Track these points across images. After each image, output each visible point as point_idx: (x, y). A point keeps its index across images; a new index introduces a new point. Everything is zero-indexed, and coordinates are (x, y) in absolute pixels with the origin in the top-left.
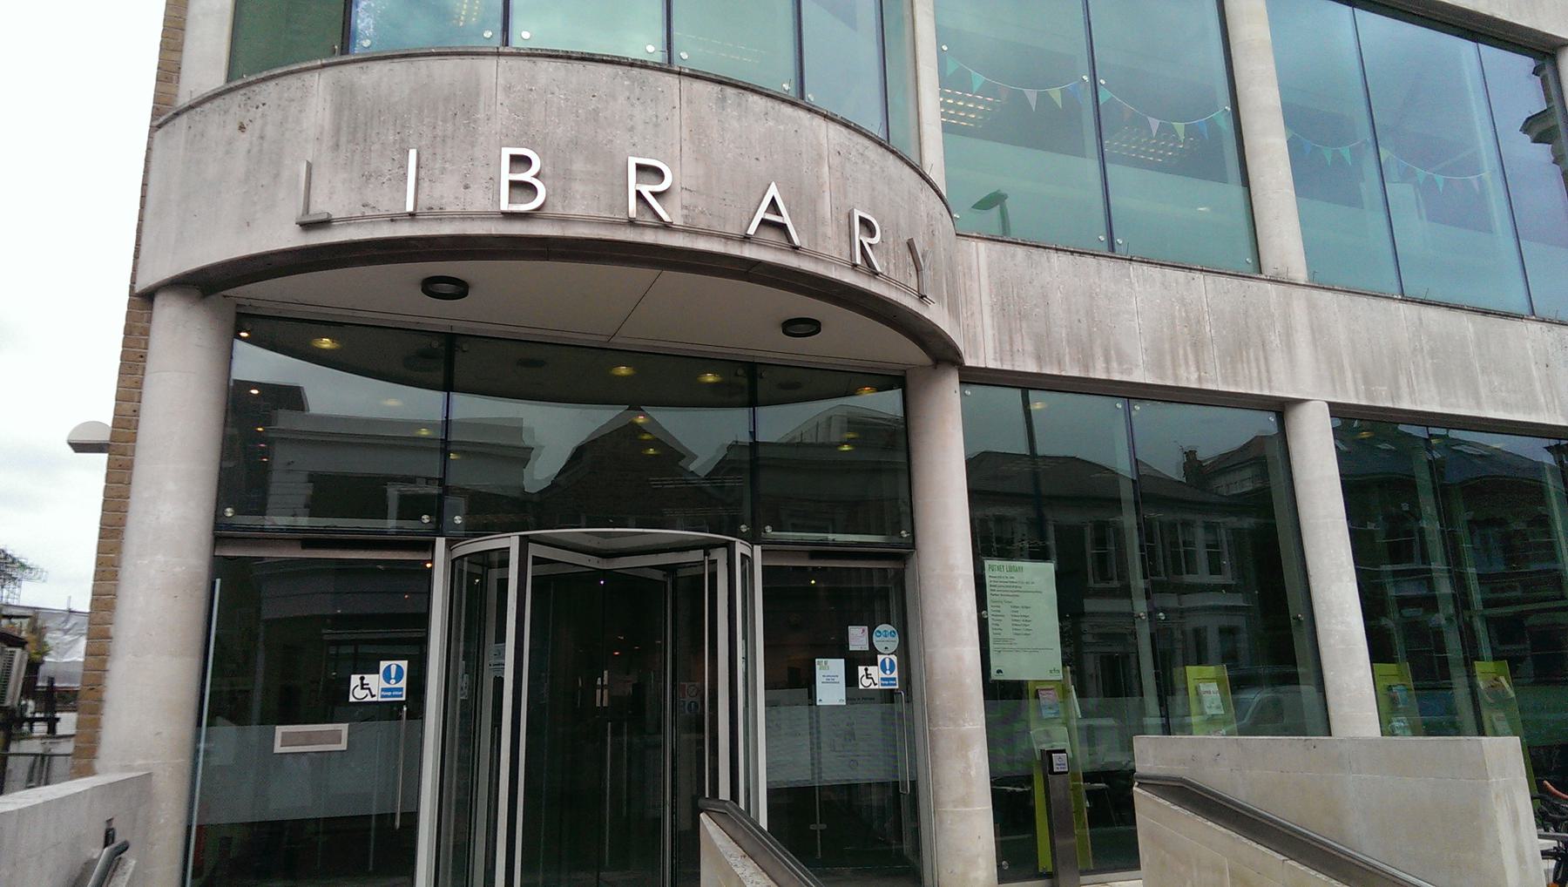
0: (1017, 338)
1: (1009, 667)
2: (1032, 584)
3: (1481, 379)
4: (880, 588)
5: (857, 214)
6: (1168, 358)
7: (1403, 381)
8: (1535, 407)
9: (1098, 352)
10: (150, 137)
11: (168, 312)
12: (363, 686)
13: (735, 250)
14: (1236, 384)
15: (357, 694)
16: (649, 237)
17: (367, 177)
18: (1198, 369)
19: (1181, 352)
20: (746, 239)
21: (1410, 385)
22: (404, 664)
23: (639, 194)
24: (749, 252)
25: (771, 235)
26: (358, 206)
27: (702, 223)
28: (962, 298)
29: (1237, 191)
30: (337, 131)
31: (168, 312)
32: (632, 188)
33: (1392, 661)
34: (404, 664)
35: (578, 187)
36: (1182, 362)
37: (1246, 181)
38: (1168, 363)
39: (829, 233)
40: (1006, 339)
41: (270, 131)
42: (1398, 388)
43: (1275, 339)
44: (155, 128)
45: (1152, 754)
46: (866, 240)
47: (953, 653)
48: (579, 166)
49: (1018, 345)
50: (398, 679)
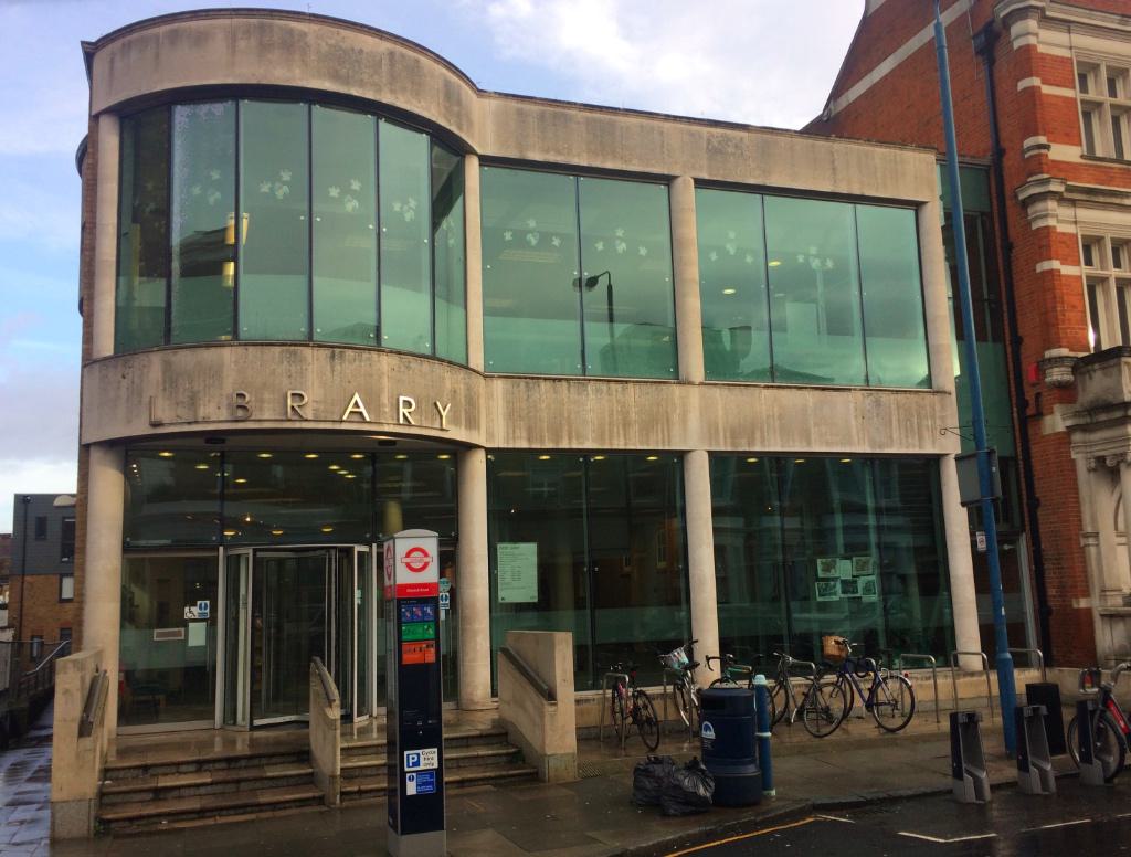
0: (518, 431)
1: (509, 595)
2: (523, 559)
3: (813, 430)
5: (402, 399)
6: (607, 433)
7: (758, 435)
8: (850, 443)
9: (565, 434)
10: (82, 371)
11: (95, 455)
12: (190, 612)
14: (648, 445)
15: (188, 615)
16: (298, 425)
17: (177, 404)
18: (625, 438)
19: (615, 429)
22: (208, 602)
23: (404, 415)
24: (344, 426)
25: (356, 418)
26: (172, 416)
30: (164, 382)
31: (95, 455)
33: (119, 724)
34: (208, 602)
36: (615, 434)
38: (607, 437)
39: (387, 410)
41: (136, 379)
43: (676, 418)
44: (84, 366)
46: (406, 411)
48: (267, 396)
50: (205, 608)
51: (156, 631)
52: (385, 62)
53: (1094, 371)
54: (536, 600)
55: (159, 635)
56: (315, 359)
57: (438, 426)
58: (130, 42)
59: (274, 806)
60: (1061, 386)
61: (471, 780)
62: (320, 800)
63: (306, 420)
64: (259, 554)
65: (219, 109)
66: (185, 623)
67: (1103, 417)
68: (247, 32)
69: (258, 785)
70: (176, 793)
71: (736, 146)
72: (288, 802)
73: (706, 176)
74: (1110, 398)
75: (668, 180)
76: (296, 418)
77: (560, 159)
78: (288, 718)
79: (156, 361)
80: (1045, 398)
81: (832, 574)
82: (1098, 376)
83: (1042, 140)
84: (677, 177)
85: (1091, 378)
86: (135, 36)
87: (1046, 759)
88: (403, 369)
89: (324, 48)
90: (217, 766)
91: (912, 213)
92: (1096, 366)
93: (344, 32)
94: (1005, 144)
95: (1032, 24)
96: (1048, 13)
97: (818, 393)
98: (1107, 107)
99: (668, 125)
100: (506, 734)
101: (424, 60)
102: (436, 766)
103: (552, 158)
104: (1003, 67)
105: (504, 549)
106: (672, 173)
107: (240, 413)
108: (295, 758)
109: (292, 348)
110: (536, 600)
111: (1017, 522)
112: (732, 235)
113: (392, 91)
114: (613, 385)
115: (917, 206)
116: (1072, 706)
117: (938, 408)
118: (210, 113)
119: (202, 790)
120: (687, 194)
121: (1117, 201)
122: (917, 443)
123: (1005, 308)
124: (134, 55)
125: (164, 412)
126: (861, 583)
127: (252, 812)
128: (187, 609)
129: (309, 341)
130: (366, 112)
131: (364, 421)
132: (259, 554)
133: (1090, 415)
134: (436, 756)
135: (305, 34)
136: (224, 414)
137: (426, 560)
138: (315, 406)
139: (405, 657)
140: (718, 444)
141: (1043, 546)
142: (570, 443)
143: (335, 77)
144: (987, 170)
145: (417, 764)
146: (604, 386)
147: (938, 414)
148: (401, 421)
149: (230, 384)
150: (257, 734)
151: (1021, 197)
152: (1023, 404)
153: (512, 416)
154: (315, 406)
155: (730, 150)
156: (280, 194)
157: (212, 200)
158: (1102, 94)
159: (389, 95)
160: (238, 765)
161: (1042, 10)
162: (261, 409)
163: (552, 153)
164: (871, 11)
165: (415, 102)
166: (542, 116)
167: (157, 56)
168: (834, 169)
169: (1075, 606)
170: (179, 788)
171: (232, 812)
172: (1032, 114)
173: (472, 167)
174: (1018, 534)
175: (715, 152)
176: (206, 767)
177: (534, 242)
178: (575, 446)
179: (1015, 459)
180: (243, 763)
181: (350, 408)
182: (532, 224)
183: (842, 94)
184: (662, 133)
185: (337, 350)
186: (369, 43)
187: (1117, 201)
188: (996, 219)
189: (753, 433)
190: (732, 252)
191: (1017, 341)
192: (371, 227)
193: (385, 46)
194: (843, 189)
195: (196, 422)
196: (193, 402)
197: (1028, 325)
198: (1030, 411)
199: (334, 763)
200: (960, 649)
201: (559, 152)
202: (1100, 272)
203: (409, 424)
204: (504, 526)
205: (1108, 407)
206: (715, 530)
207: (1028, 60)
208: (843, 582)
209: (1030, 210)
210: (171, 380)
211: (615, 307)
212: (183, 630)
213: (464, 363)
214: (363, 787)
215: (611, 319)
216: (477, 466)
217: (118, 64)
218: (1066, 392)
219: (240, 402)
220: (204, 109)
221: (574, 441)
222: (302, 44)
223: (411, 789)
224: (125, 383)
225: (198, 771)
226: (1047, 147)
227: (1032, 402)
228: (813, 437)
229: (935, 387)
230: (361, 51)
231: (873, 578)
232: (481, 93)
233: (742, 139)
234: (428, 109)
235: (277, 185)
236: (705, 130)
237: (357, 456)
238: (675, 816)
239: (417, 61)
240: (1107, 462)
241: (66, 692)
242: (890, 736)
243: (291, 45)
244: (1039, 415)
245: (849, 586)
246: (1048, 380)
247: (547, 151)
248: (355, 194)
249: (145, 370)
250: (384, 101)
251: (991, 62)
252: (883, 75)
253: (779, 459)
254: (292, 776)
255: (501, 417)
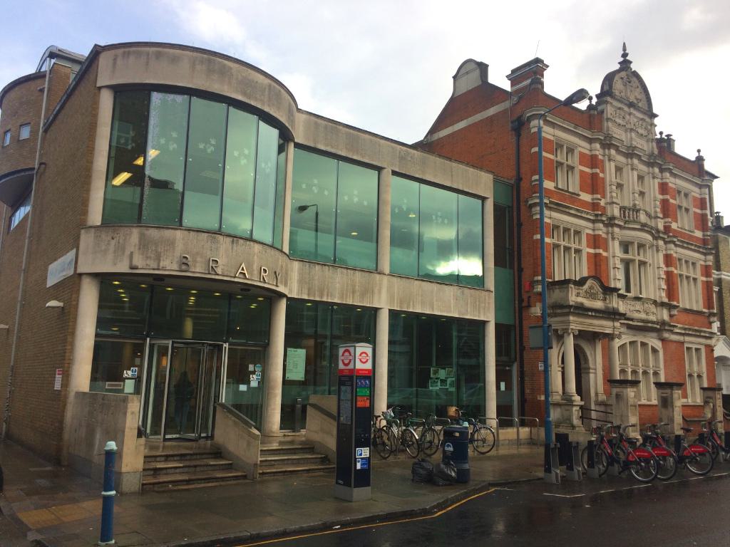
0: (303, 289)
1: (290, 376)
2: (299, 356)
4: (262, 355)
5: (263, 268)
7: (411, 303)
8: (450, 312)
9: (325, 293)
13: (233, 279)
15: (125, 375)
16: (213, 277)
17: (147, 258)
20: (235, 277)
21: (413, 304)
23: (212, 267)
24: (236, 280)
25: (241, 276)
26: (144, 265)
27: (226, 273)
28: (289, 278)
29: (375, 244)
30: (140, 245)
32: (211, 265)
34: (137, 368)
35: (198, 265)
36: (187, 463)
37: (377, 242)
40: (300, 291)
41: (121, 241)
42: (410, 305)
43: (376, 291)
45: (313, 399)
47: (277, 374)
48: (199, 259)
49: (303, 291)
51: (107, 383)
52: (267, 90)
53: (556, 288)
54: (303, 379)
55: (109, 385)
56: (224, 243)
57: (275, 284)
58: (129, 53)
59: (223, 479)
60: (540, 294)
61: (313, 469)
62: (245, 477)
63: (218, 275)
64: (175, 345)
65: (180, 99)
66: (123, 380)
67: (559, 311)
68: (202, 62)
69: (206, 468)
70: (165, 471)
71: (411, 157)
72: (229, 477)
73: (397, 170)
74: (562, 302)
75: (380, 169)
76: (213, 273)
77: (333, 151)
78: (174, 436)
79: (135, 235)
80: (532, 299)
81: (437, 376)
82: (557, 291)
83: (670, 220)
84: (384, 168)
85: (553, 291)
86: (132, 49)
87: (557, 468)
88: (264, 252)
89: (240, 77)
90: (175, 458)
91: (480, 201)
92: (557, 287)
93: (250, 71)
94: (523, 176)
95: (668, 174)
96: (548, 118)
97: (438, 285)
98: (565, 166)
99: (383, 142)
100: (313, 448)
101: (282, 91)
102: (368, 456)
103: (329, 149)
104: (524, 141)
105: (291, 351)
106: (383, 166)
107: (184, 267)
108: (213, 456)
109: (213, 235)
110: (303, 379)
111: (513, 356)
112: (405, 201)
113: (269, 106)
114: (349, 271)
115: (483, 199)
116: (541, 445)
117: (487, 298)
118: (174, 100)
119: (178, 471)
120: (387, 173)
121: (567, 210)
122: (477, 314)
123: (516, 253)
124: (132, 59)
125: (139, 261)
126: (449, 381)
127: (213, 482)
128: (125, 372)
129: (219, 232)
130: (254, 114)
131: (246, 278)
132: (175, 345)
133: (553, 309)
134: (368, 451)
135: (231, 68)
136: (175, 267)
137: (368, 358)
138: (223, 267)
139: (358, 403)
140: (394, 306)
141: (525, 369)
142: (327, 298)
143: (244, 94)
144: (512, 186)
145: (361, 455)
146: (345, 271)
147: (487, 301)
148: (262, 280)
149: (179, 249)
150: (167, 443)
151: (530, 203)
152: (521, 301)
153: (301, 281)
154: (223, 267)
155: (410, 159)
156: (209, 151)
157: (171, 148)
158: (563, 159)
159: (268, 108)
160: (186, 458)
161: (640, 156)
162: (195, 266)
163: (367, 157)
164: (456, 95)
165: (277, 112)
166: (326, 127)
167: (147, 64)
168: (452, 176)
169: (538, 399)
170: (166, 468)
171: (203, 481)
172: (537, 165)
173: (292, 145)
174: (513, 362)
175: (402, 158)
176: (169, 459)
177: (316, 191)
178: (330, 301)
179: (515, 326)
180: (188, 457)
181: (240, 271)
182: (316, 181)
183: (436, 132)
184: (379, 145)
185: (235, 239)
186: (261, 78)
187: (567, 210)
188: (515, 209)
189: (410, 302)
190: (405, 209)
191: (520, 270)
192: (220, 165)
193: (267, 81)
194: (455, 186)
195: (158, 269)
196: (158, 259)
197: (527, 262)
198: (524, 304)
199: (257, 458)
200: (487, 416)
201: (332, 147)
202: (631, 257)
203: (265, 282)
204: (292, 340)
205: (562, 307)
206: (390, 352)
207: (537, 139)
208: (441, 380)
209: (533, 209)
210: (144, 244)
211: (319, 225)
212: (122, 383)
213: (280, 248)
214: (265, 471)
215: (317, 231)
216: (282, 307)
217: (119, 62)
218: (541, 295)
219: (184, 260)
220: (171, 97)
221: (482, 314)
222: (229, 73)
223: (359, 466)
224: (113, 242)
225: (166, 461)
226: (600, 200)
227: (526, 300)
228: (435, 307)
229: (486, 288)
230: (257, 82)
231: (454, 379)
232: (299, 110)
233: (414, 154)
234: (282, 116)
235: (208, 145)
236: (399, 147)
237: (169, 289)
238: (442, 486)
239: (280, 91)
240: (559, 332)
241: (133, 413)
242: (482, 456)
243: (223, 72)
244: (529, 306)
245: (444, 382)
246: (535, 290)
247: (327, 145)
248: (246, 157)
249: (128, 237)
250: (265, 110)
251: (519, 135)
252: (459, 128)
253: (418, 315)
254: (222, 465)
255: (296, 281)
